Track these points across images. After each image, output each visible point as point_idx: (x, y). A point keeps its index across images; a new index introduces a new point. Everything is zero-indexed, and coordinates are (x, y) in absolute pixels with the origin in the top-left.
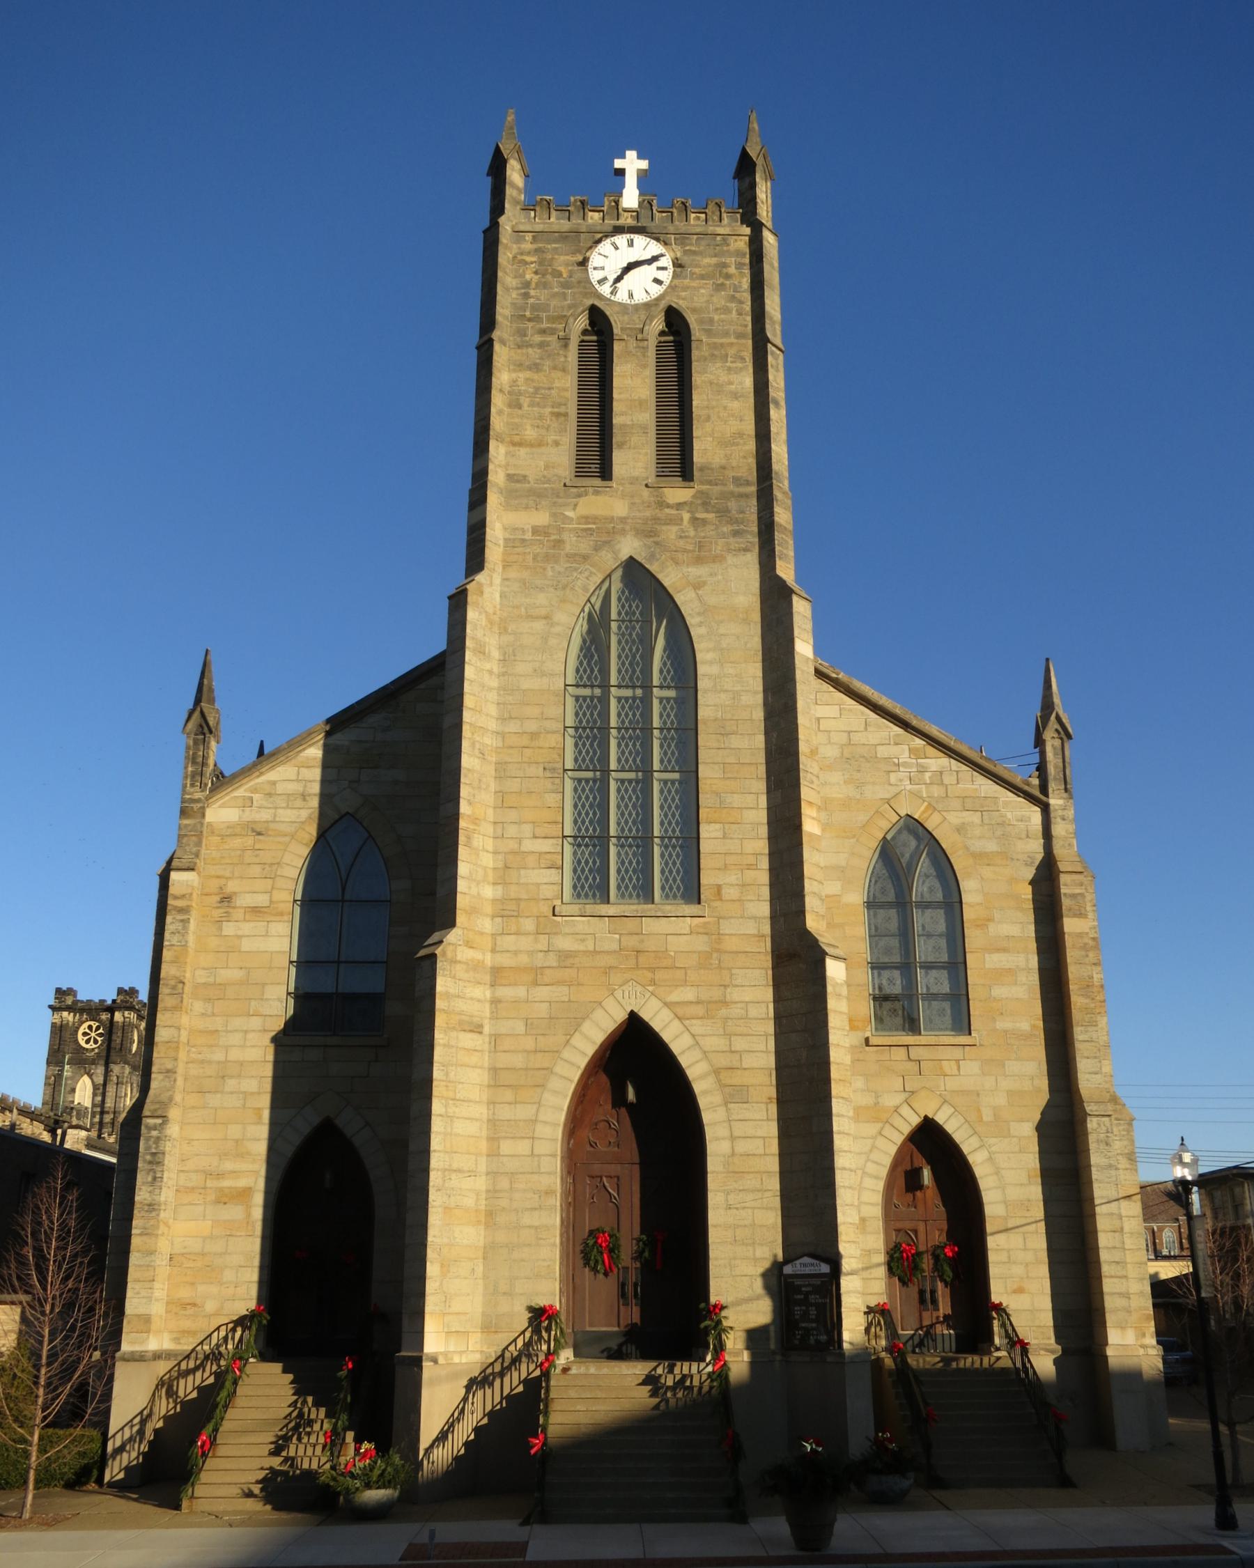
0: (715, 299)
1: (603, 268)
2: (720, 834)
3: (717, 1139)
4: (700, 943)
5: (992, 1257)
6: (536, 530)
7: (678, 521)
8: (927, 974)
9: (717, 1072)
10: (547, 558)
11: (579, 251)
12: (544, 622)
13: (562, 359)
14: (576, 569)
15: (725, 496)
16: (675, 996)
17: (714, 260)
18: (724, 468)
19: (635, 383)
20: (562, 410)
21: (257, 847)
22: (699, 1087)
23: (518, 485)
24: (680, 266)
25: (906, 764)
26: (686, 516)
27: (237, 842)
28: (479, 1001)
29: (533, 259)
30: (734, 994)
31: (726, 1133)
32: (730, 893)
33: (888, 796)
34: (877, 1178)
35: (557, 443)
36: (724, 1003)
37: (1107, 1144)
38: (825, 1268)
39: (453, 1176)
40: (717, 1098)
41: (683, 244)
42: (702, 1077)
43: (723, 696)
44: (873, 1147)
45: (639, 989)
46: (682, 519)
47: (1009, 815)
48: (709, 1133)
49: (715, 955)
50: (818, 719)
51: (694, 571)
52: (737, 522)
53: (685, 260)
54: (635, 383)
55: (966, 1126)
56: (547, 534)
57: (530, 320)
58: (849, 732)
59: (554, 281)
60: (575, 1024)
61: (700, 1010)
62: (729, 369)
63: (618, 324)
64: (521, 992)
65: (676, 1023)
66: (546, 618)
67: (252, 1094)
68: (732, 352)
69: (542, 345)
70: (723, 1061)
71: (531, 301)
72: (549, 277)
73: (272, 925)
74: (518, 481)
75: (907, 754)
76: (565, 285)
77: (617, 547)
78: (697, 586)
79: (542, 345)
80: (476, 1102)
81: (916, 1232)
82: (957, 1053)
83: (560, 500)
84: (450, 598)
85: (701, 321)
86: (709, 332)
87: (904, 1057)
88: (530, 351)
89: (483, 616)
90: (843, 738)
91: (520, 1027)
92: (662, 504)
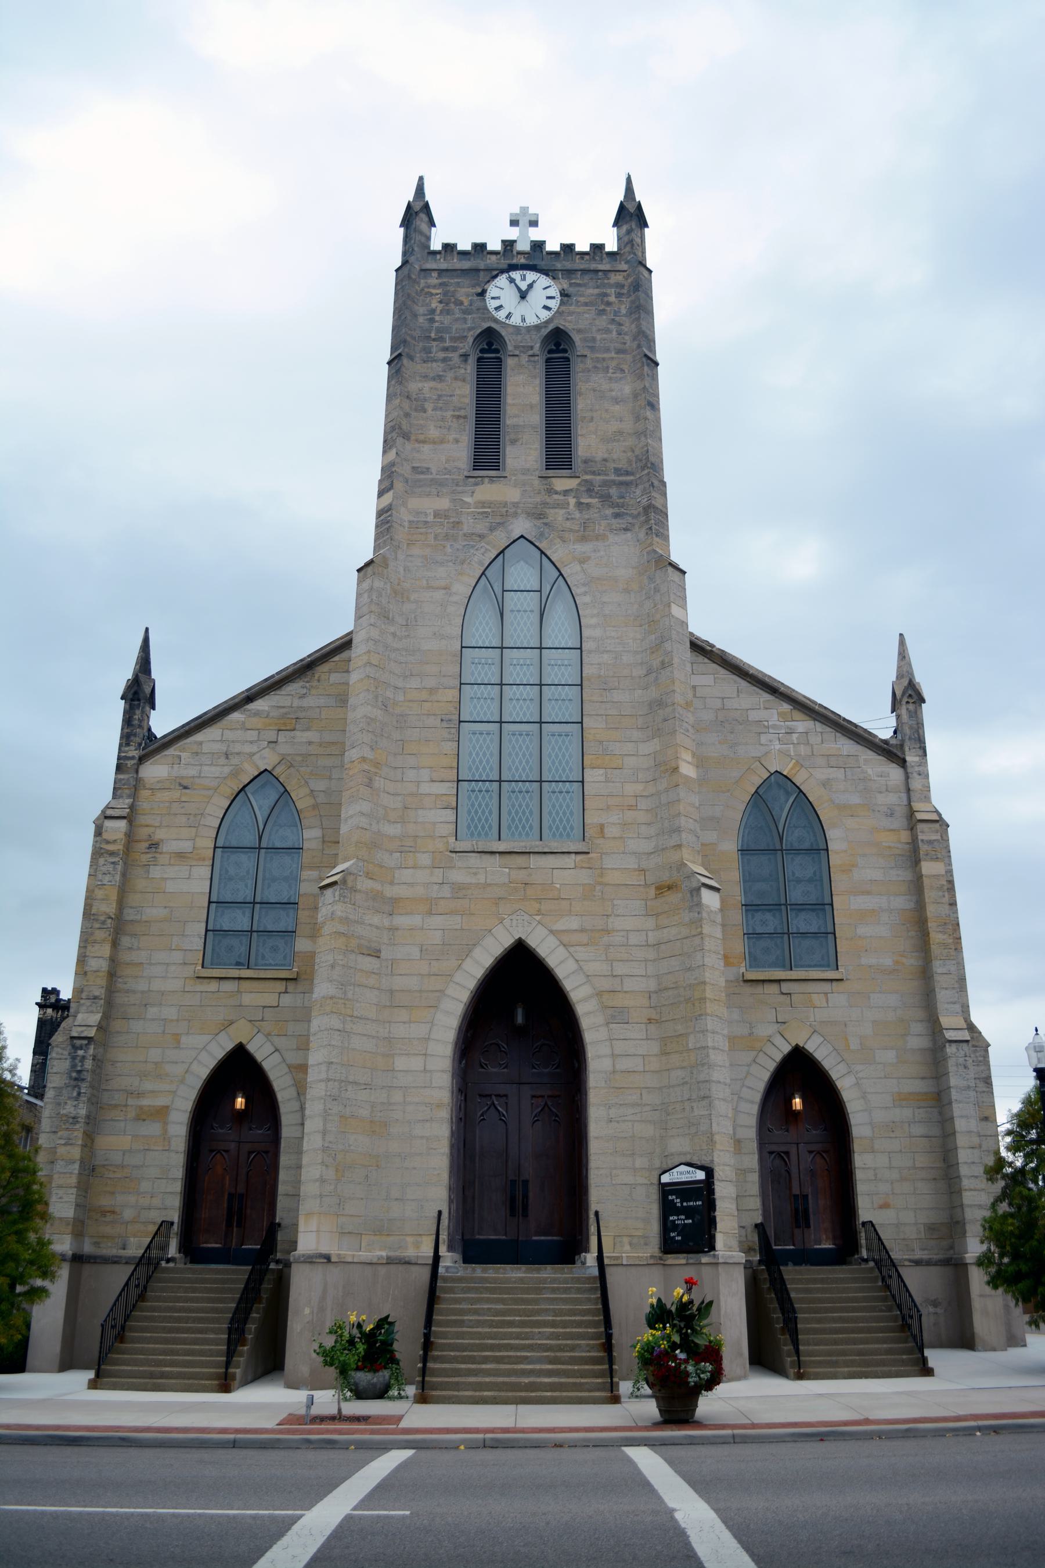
0: (597, 322)
1: (498, 298)
2: (603, 779)
3: (599, 1057)
4: (584, 877)
5: (859, 1175)
6: (436, 514)
7: (565, 505)
8: (797, 916)
9: (599, 994)
10: (447, 537)
11: (479, 285)
12: (444, 592)
13: (463, 371)
14: (473, 546)
15: (606, 484)
16: (559, 926)
17: (596, 291)
18: (605, 460)
19: (523, 392)
20: (462, 413)
21: (183, 799)
22: (581, 1009)
23: (422, 476)
24: (567, 295)
25: (774, 727)
26: (572, 501)
27: (166, 796)
28: (377, 928)
29: (438, 291)
30: (616, 923)
31: (608, 1051)
32: (611, 831)
33: (759, 755)
34: (752, 1102)
35: (457, 441)
36: (607, 931)
37: (965, 1067)
38: (701, 1175)
39: (350, 1088)
40: (600, 1019)
41: (570, 279)
42: (585, 999)
43: (606, 656)
44: (748, 1073)
45: (526, 917)
46: (568, 504)
47: (870, 771)
48: (591, 1052)
49: (598, 888)
50: (694, 687)
51: (581, 548)
52: (618, 506)
53: (571, 290)
54: (523, 392)
55: (835, 1053)
56: (446, 517)
57: (434, 340)
58: (723, 699)
59: (457, 309)
60: (467, 951)
61: (584, 938)
62: (610, 379)
63: (511, 342)
64: (416, 920)
65: (561, 949)
66: (445, 588)
67: (172, 1020)
68: (613, 364)
69: (444, 360)
70: (605, 984)
71: (437, 324)
72: (452, 306)
73: (194, 869)
74: (422, 473)
75: (776, 717)
76: (465, 312)
77: (510, 528)
78: (582, 561)
79: (444, 360)
80: (374, 1021)
81: (787, 1153)
82: (826, 987)
83: (459, 489)
84: (359, 571)
85: (585, 340)
86: (592, 349)
87: (777, 991)
88: (434, 364)
89: (388, 586)
90: (718, 704)
91: (415, 952)
92: (551, 491)
